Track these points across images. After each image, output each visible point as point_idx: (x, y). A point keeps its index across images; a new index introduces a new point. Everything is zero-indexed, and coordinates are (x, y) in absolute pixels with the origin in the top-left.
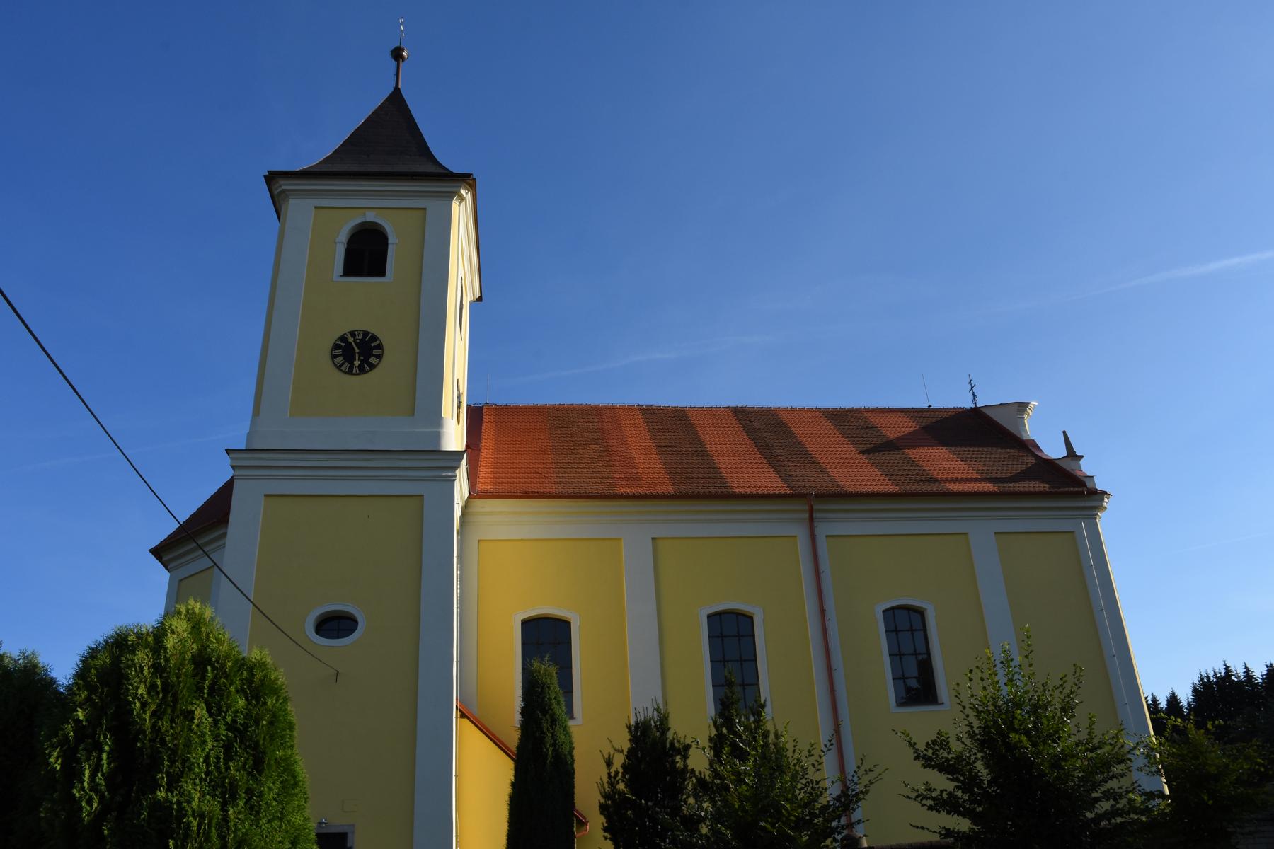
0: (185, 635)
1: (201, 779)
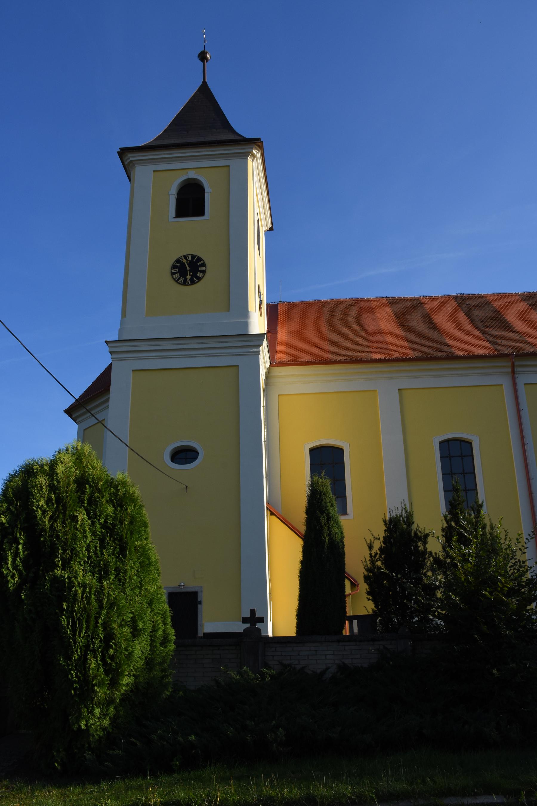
0: (70, 464)
1: (84, 562)
